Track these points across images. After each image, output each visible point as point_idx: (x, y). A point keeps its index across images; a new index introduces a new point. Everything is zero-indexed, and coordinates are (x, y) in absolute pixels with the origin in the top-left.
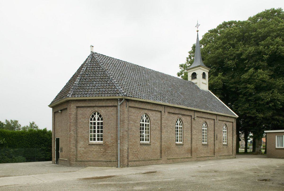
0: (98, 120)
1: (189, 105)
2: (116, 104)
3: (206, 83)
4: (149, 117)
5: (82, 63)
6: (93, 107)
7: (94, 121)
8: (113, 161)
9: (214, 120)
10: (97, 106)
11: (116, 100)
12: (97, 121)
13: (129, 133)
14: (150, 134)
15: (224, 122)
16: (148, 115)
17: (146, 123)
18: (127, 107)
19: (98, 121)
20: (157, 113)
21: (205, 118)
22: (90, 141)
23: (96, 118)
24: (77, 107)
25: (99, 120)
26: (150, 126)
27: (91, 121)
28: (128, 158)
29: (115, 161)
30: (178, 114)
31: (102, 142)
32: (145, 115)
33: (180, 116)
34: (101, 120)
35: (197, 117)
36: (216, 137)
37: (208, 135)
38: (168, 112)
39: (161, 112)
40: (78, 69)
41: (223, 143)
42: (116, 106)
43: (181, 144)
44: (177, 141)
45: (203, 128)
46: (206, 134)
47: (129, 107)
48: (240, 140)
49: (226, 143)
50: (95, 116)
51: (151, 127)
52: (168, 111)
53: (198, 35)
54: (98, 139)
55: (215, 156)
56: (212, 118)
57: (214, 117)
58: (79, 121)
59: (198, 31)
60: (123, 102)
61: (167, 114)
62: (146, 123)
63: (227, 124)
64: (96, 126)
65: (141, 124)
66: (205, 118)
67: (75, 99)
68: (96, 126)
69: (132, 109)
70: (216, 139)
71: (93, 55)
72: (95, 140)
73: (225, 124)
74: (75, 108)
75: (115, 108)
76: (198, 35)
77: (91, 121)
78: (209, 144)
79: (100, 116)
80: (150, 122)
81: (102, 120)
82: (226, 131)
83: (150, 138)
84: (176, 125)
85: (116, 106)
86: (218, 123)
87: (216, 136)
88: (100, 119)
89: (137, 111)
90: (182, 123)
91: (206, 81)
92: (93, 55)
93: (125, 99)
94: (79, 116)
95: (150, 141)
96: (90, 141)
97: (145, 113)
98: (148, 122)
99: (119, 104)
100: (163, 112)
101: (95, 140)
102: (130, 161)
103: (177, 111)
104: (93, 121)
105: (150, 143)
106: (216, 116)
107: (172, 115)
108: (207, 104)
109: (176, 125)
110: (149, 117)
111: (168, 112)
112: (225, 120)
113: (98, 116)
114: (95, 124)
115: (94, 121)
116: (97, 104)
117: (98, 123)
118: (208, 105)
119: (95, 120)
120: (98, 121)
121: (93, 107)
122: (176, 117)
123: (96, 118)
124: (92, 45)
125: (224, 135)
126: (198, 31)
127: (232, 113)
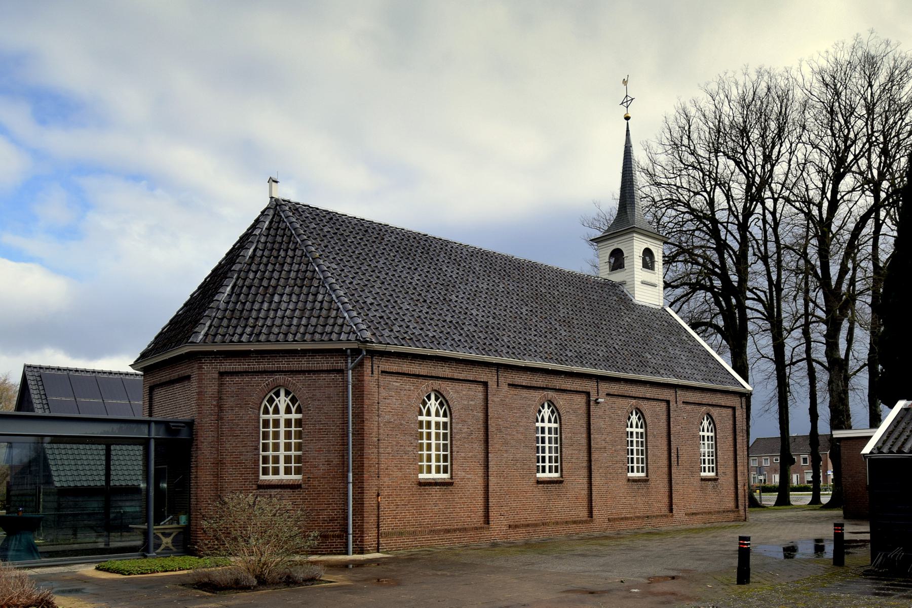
0: (288, 411)
1: (580, 358)
2: (340, 365)
3: (656, 282)
4: (447, 401)
5: (244, 231)
6: (272, 372)
7: (276, 416)
8: (333, 536)
9: (668, 402)
10: (282, 372)
11: (341, 352)
12: (283, 416)
13: (381, 450)
14: (451, 452)
15: (704, 409)
16: (444, 394)
17: (438, 419)
18: (376, 372)
19: (288, 416)
20: (473, 386)
21: (635, 398)
22: (262, 477)
23: (282, 408)
24: (222, 374)
25: (291, 413)
26: (451, 428)
27: (266, 417)
28: (378, 527)
29: (339, 536)
30: (543, 389)
31: (299, 477)
32: (436, 396)
33: (551, 394)
34: (296, 413)
35: (608, 395)
36: (674, 455)
37: (647, 449)
38: (509, 385)
39: (485, 384)
40: (228, 250)
41: (703, 474)
42: (341, 371)
43: (273, 483)
44: (632, 471)
45: (629, 429)
46: (640, 448)
47: (382, 372)
48: (793, 462)
49: (643, 475)
50: (277, 400)
51: (454, 430)
52: (510, 381)
53: (628, 131)
54: (288, 471)
55: (672, 516)
56: (661, 397)
57: (667, 394)
58: (228, 415)
59: (627, 118)
60: (362, 359)
61: (505, 388)
62: (438, 419)
63: (715, 412)
64: (282, 429)
65: (421, 422)
66: (635, 398)
67: (215, 348)
68: (282, 429)
69: (389, 378)
70: (674, 462)
71: (277, 207)
72: (276, 471)
73: (708, 414)
74: (216, 376)
75: (339, 377)
76: (628, 131)
77: (266, 417)
78: (456, 481)
79: (294, 400)
80: (451, 414)
81: (299, 411)
82: (712, 434)
83: (452, 465)
84: (537, 421)
85: (341, 371)
86: (680, 414)
87: (674, 451)
88: (293, 410)
89: (408, 385)
90: (559, 415)
91: (658, 275)
92: (277, 207)
93: (367, 351)
94: (229, 402)
95: (451, 474)
96: (262, 477)
97: (436, 390)
98: (445, 415)
99: (350, 365)
100: (492, 385)
101: (276, 471)
102: (387, 535)
103: (539, 380)
104: (271, 417)
105: (451, 478)
106: (672, 392)
107: (525, 393)
108: (647, 354)
109: (537, 421)
110: (447, 401)
111: (509, 385)
112: (705, 401)
113: (288, 400)
114: (276, 423)
115: (276, 416)
116: (284, 364)
117: (288, 423)
118: (649, 357)
119: (276, 411)
120: (288, 416)
121: (272, 372)
122: (537, 395)
123: (282, 408)
124: (275, 177)
125: (705, 449)
126: (627, 118)
127: (734, 378)
